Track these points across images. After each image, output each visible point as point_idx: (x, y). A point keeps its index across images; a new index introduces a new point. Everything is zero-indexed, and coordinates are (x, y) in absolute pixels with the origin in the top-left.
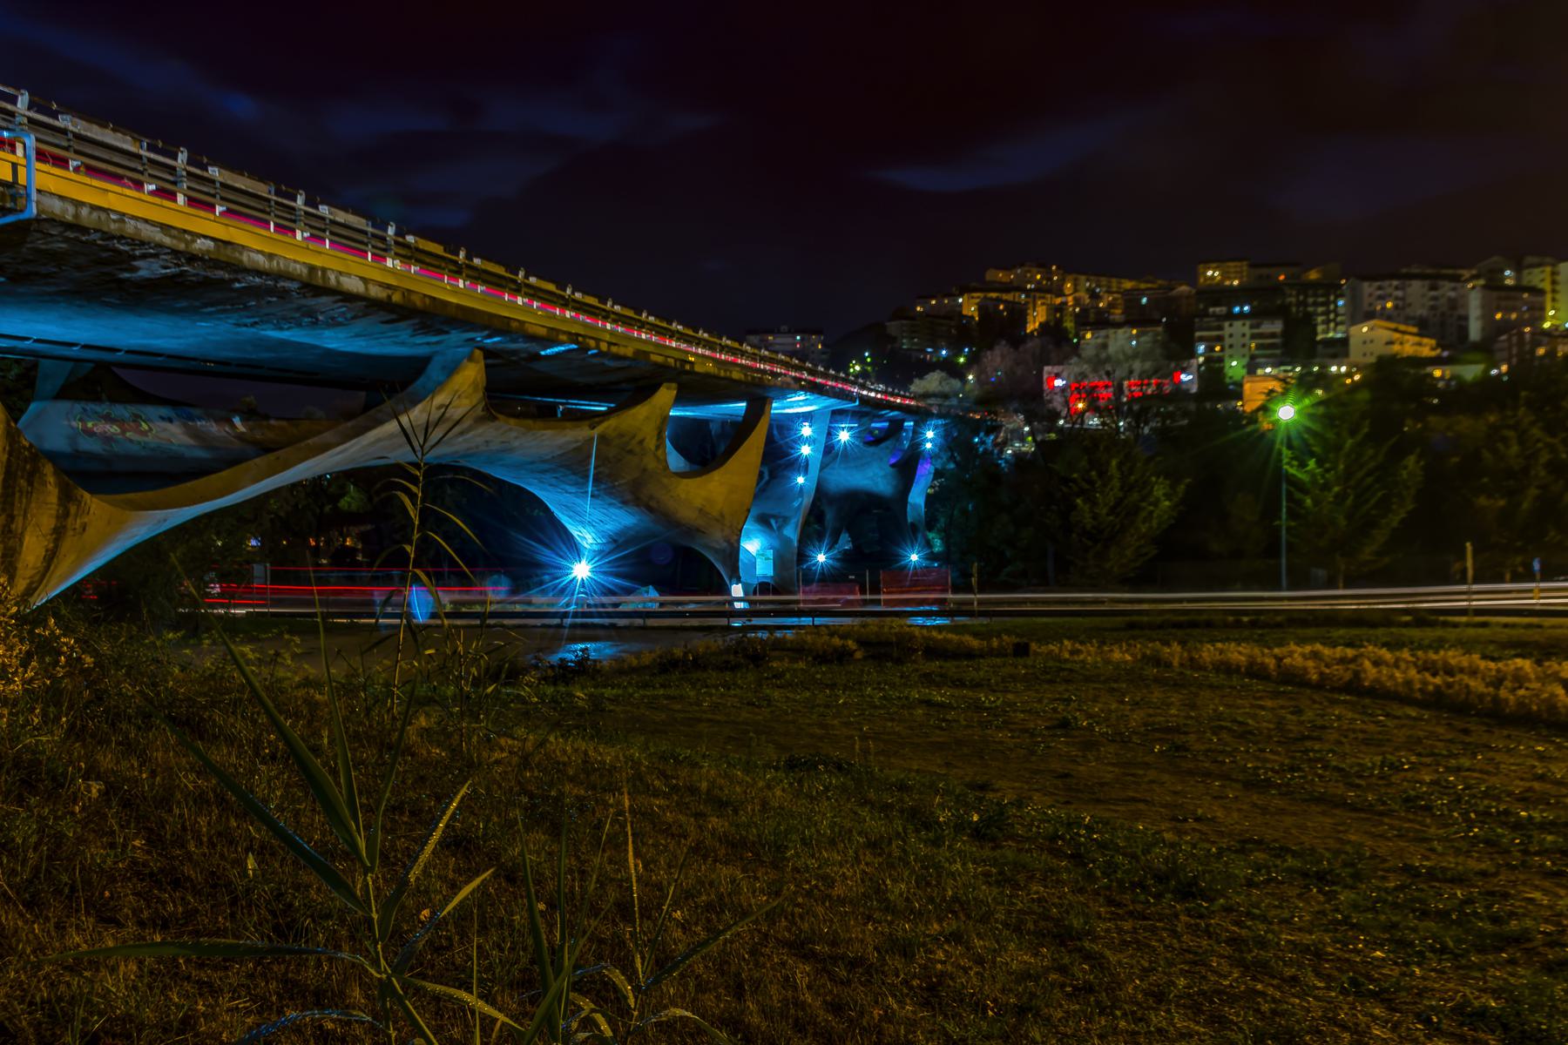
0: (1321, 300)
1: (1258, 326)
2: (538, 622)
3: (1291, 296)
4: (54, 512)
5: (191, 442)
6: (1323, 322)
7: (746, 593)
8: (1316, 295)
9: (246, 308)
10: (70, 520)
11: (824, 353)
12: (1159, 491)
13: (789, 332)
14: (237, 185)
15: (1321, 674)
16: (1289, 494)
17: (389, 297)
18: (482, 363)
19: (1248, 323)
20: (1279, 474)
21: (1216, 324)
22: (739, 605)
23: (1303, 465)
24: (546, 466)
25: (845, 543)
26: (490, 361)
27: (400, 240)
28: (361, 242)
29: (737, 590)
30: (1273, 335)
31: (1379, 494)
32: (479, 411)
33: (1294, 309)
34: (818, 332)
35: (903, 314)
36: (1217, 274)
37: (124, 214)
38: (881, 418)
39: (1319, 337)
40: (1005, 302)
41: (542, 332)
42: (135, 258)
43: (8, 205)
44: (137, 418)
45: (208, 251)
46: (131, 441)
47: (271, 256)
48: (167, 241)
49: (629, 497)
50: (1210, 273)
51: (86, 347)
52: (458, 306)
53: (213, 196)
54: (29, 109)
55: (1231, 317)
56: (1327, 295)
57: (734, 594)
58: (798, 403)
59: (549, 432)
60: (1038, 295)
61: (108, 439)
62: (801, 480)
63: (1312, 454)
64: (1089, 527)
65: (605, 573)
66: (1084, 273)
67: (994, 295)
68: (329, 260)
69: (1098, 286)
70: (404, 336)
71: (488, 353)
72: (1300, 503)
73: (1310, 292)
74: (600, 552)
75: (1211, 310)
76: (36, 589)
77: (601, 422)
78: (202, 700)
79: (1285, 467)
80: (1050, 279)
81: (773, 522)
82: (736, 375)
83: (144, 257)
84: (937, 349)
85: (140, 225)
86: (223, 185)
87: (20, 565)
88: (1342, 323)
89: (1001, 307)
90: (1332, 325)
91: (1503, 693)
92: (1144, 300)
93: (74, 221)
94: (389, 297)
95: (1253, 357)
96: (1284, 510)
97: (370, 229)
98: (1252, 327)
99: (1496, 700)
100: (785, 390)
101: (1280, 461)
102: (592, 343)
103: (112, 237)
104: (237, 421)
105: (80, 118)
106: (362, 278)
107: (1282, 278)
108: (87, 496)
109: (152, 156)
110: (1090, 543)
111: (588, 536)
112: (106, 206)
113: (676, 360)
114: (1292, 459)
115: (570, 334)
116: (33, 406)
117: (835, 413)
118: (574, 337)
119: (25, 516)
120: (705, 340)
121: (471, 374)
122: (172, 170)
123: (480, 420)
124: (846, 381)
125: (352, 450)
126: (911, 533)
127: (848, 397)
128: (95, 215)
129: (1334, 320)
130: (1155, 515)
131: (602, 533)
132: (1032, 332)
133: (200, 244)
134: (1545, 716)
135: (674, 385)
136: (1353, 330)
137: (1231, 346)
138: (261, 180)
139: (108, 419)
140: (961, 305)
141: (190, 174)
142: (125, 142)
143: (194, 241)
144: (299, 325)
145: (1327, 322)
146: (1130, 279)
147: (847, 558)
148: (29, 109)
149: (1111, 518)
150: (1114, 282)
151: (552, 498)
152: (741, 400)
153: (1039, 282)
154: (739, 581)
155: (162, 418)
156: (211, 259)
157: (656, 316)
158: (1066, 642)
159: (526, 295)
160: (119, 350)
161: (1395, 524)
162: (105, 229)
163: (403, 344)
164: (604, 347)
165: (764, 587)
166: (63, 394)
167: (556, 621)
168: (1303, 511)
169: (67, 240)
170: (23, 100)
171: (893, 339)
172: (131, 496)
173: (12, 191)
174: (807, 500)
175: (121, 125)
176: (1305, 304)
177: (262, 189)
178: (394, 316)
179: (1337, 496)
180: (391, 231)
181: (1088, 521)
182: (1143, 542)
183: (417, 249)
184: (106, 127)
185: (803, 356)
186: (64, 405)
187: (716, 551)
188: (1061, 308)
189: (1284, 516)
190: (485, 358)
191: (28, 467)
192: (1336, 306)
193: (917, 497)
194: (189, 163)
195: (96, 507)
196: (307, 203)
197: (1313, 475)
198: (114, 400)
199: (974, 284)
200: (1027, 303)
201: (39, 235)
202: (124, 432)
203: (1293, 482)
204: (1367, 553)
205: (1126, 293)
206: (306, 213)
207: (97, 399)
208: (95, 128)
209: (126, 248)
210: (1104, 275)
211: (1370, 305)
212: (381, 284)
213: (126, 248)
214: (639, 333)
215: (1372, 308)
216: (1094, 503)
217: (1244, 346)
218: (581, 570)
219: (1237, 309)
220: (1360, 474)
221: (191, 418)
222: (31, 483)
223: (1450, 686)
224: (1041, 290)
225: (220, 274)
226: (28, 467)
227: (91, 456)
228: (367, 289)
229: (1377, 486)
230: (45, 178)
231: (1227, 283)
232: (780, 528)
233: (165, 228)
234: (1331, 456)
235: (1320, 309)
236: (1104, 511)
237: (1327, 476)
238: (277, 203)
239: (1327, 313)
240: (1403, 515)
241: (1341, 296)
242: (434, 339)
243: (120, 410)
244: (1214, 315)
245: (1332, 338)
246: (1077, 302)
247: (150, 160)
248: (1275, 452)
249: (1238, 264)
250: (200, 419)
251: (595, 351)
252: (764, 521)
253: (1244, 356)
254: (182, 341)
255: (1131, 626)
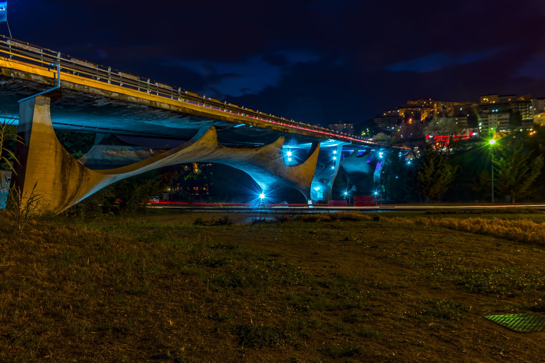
0: (524, 107)
1: (500, 116)
2: (245, 211)
3: (513, 106)
4: (78, 174)
5: (136, 156)
6: (525, 114)
7: (312, 203)
8: (522, 105)
9: (135, 114)
10: (84, 177)
11: (353, 129)
12: (447, 169)
13: (342, 123)
14: (127, 77)
15: (471, 227)
16: (494, 170)
17: (178, 110)
18: (215, 130)
19: (497, 115)
20: (491, 163)
21: (485, 116)
22: (310, 207)
23: (499, 160)
24: (245, 163)
25: (354, 189)
26: (218, 130)
27: (182, 92)
28: (169, 94)
29: (310, 202)
30: (506, 119)
31: (527, 169)
32: (216, 145)
33: (514, 110)
34: (351, 123)
35: (380, 116)
36: (487, 99)
37: (89, 86)
38: (363, 148)
39: (523, 119)
40: (414, 111)
41: (233, 120)
42: (95, 100)
43: (53, 84)
44: (122, 150)
45: (116, 97)
46: (119, 156)
47: (137, 98)
48: (103, 94)
49: (273, 173)
50: (484, 99)
51: (100, 128)
52: (202, 113)
53: (120, 81)
54: (61, 57)
55: (491, 113)
56: (526, 105)
57: (309, 203)
58: (331, 143)
59: (242, 152)
60: (425, 108)
61: (113, 155)
62: (333, 168)
63: (502, 156)
64: (423, 181)
65: (270, 197)
66: (440, 101)
67: (410, 109)
68: (157, 99)
69: (446, 105)
70: (187, 122)
71: (217, 128)
72: (497, 173)
73: (520, 104)
74: (268, 190)
75: (484, 111)
76: (74, 197)
77: (259, 149)
78: (162, 232)
79: (493, 161)
80: (429, 103)
81: (324, 181)
82: (304, 134)
83: (97, 99)
84: (391, 127)
85: (94, 90)
86: (123, 77)
87: (68, 189)
88: (531, 114)
89: (412, 113)
90: (528, 115)
91: (527, 233)
92: (461, 109)
93: (73, 89)
94: (178, 110)
95: (499, 127)
96: (493, 175)
97: (172, 90)
98: (498, 116)
99: (525, 236)
100: (325, 138)
101: (491, 159)
102: (251, 124)
103: (86, 93)
104: (151, 150)
105: (77, 59)
106: (168, 104)
107: (510, 100)
108: (89, 170)
109: (99, 69)
110: (423, 187)
111: (263, 185)
112: (83, 84)
113: (281, 129)
114: (495, 158)
115: (242, 121)
116: (93, 147)
117: (344, 146)
118: (243, 122)
119: (69, 175)
120: (293, 123)
121: (211, 134)
122: (107, 73)
123: (217, 148)
124: (360, 139)
125: (175, 157)
126: (376, 185)
127: (348, 141)
128: (80, 87)
129: (528, 113)
130: (446, 177)
131: (267, 184)
132: (423, 120)
133: (114, 95)
134: (541, 242)
135: (284, 137)
136: (535, 116)
137: (491, 123)
138: (135, 76)
139: (114, 150)
140: (399, 112)
141: (111, 74)
142: (91, 66)
143: (112, 94)
144: (154, 119)
145: (526, 114)
146: (457, 102)
147: (354, 193)
148: (61, 57)
149: (431, 178)
150: (451, 103)
151: (252, 174)
152: (310, 143)
153: (425, 104)
154: (310, 199)
155: (129, 150)
156: (117, 99)
157: (275, 115)
158: (397, 217)
159: (244, 113)
160: (110, 129)
161: (533, 180)
162: (83, 91)
163: (188, 125)
164: (255, 125)
165: (320, 202)
166: (101, 143)
167: (250, 211)
168: (499, 176)
169: (73, 94)
170: (59, 55)
171: (376, 124)
172: (105, 170)
173: (54, 80)
174: (335, 174)
175: (89, 61)
176: (518, 108)
177: (135, 78)
178: (181, 116)
179: (511, 170)
180: (179, 90)
181: (423, 180)
182: (442, 186)
183: (188, 95)
184: (85, 62)
185: (344, 131)
186: (102, 146)
187: (303, 190)
188: (432, 113)
189: (493, 178)
190: (216, 129)
191: (69, 161)
192: (529, 109)
193: (377, 174)
194: (111, 71)
195: (92, 173)
196: (150, 82)
197: (502, 163)
198: (115, 145)
199: (403, 106)
200: (421, 111)
201: (65, 93)
202: (117, 154)
203: (496, 166)
204: (523, 189)
205: (454, 107)
206: (150, 85)
207: (111, 144)
208: (82, 62)
209: (92, 96)
210: (447, 101)
211: (542, 108)
212: (175, 106)
213: (92, 96)
214: (280, 123)
215: (542, 109)
216: (425, 173)
217: (495, 123)
218: (262, 196)
219: (493, 111)
220: (521, 162)
221: (138, 150)
222: (70, 166)
223: (510, 231)
224: (426, 107)
225: (122, 104)
226: (69, 161)
227: (107, 161)
228: (170, 107)
229: (526, 167)
230: (64, 77)
231: (491, 102)
232: (327, 183)
233: (102, 90)
234: (510, 156)
235: (523, 110)
236: (429, 176)
237: (508, 163)
238: (140, 82)
239: (526, 111)
240: (536, 176)
241: (531, 105)
242: (198, 123)
243: (118, 148)
244: (485, 113)
245: (528, 120)
246: (438, 110)
247: (99, 71)
248: (489, 156)
249: (495, 96)
250: (140, 150)
251: (252, 126)
252: (322, 181)
253: (495, 126)
254: (124, 126)
255: (428, 213)
